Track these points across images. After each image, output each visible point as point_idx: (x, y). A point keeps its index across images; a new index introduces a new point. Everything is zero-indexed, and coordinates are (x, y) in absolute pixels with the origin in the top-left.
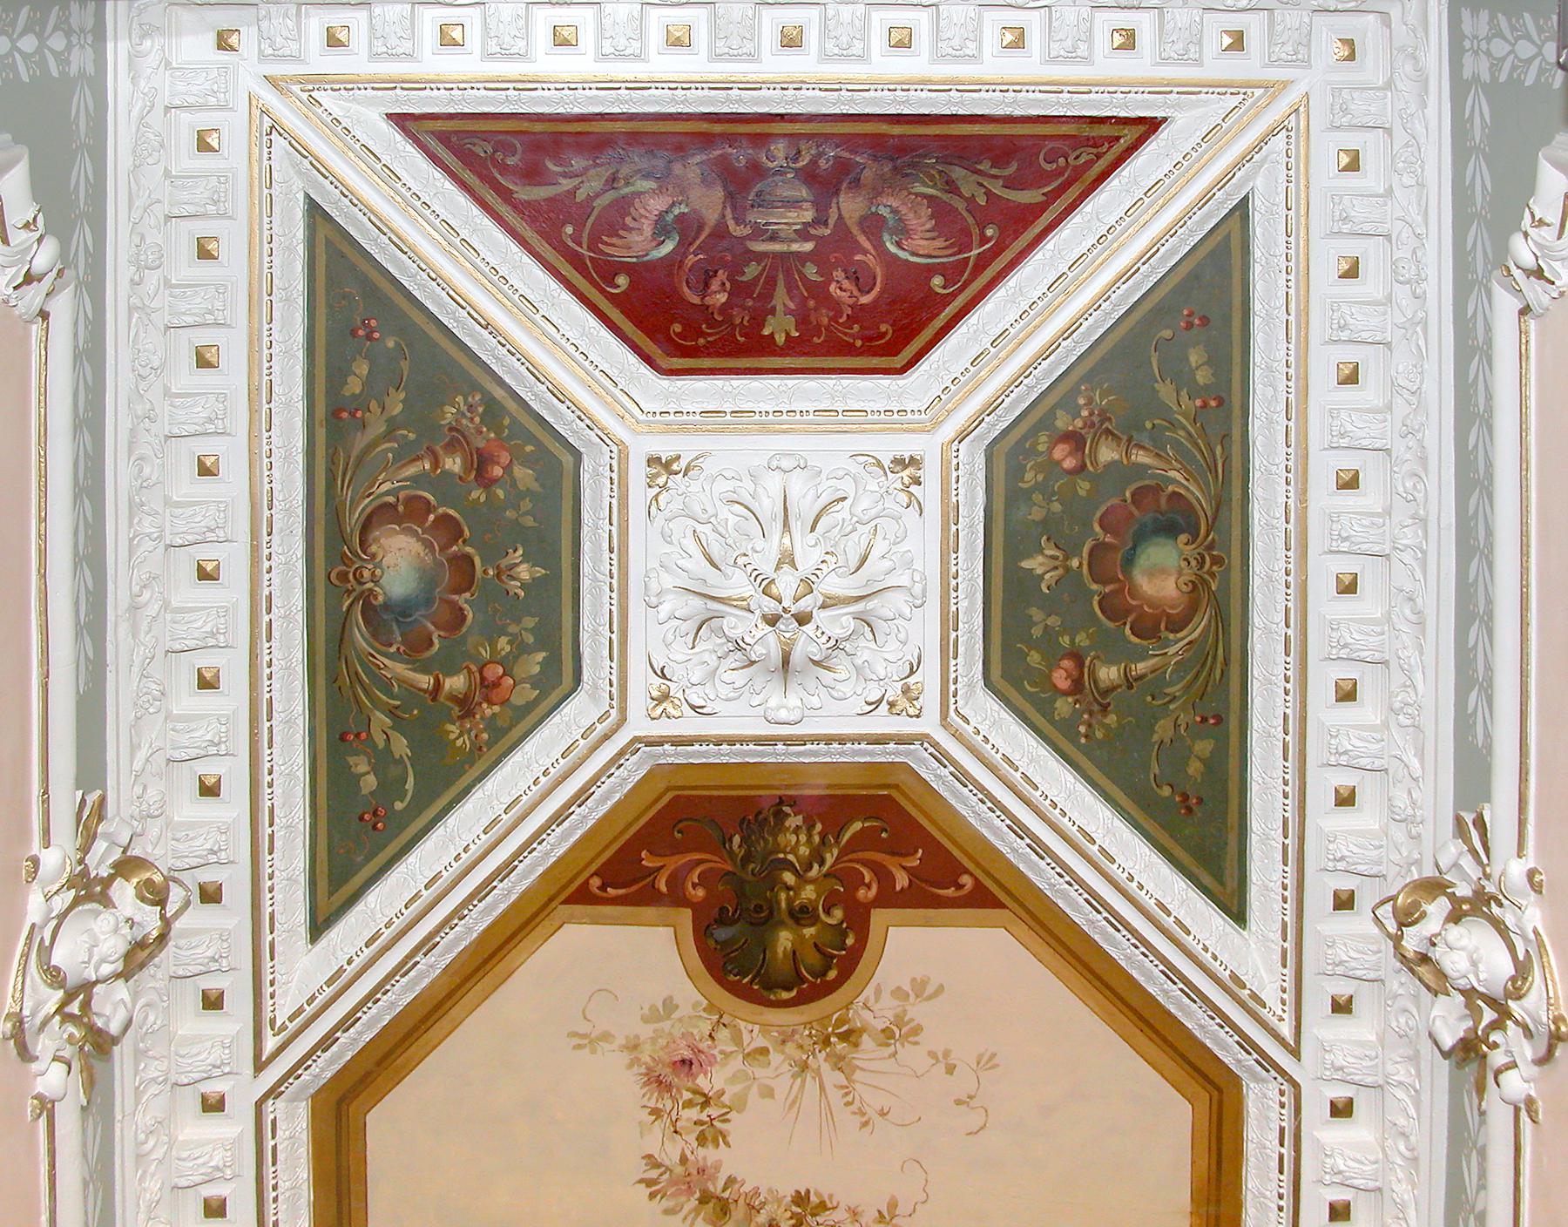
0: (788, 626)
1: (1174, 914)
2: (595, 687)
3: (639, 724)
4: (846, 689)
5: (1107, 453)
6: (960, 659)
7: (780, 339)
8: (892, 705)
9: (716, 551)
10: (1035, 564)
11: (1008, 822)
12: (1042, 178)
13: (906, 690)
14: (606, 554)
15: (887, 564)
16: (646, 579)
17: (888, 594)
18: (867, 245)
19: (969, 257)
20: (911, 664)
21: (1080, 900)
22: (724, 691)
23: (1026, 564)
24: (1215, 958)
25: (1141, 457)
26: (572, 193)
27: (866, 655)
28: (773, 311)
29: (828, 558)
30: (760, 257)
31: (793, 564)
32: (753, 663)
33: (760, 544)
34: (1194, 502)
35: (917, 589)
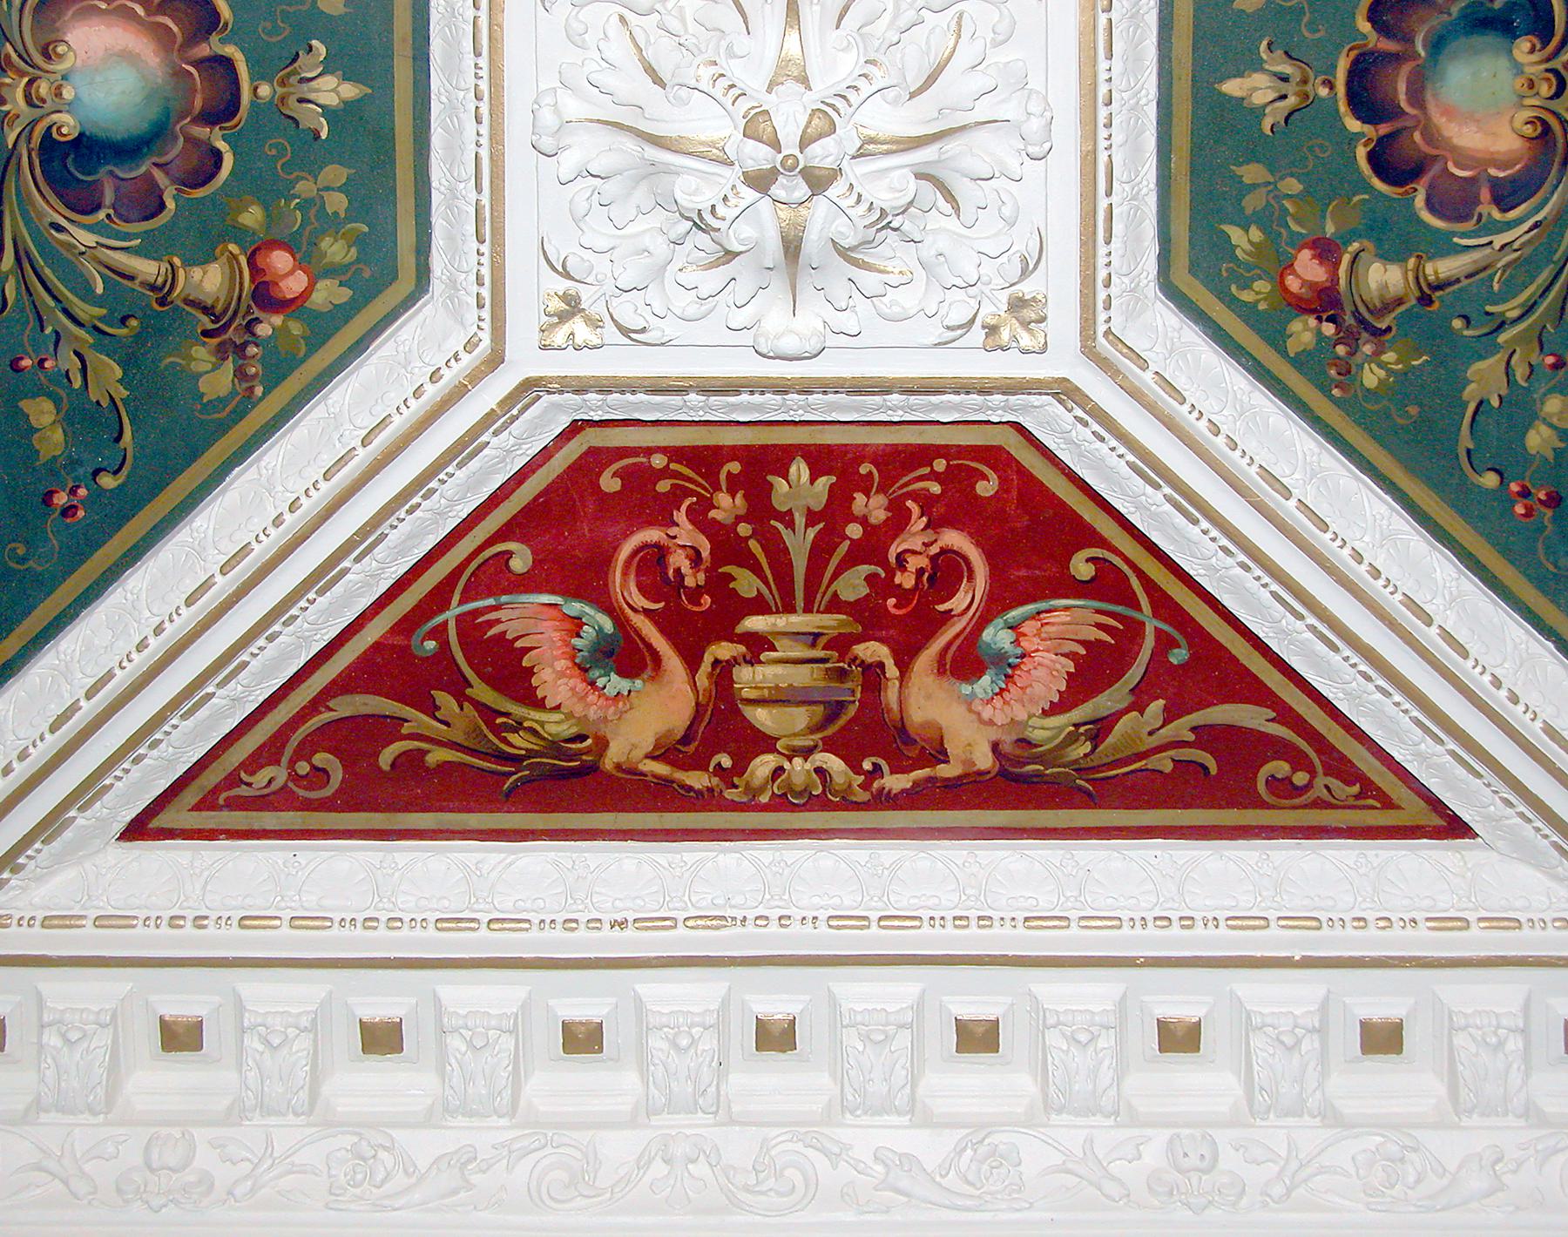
0: (791, 188)
1: (1438, 620)
2: (453, 284)
3: (524, 361)
4: (906, 299)
5: (210, 281)
6: (1116, 243)
7: (800, 469)
8: (992, 330)
9: (665, 57)
10: (331, 91)
11: (1130, 458)
12: (330, 737)
13: (1018, 305)
14: (470, 59)
15: (980, 82)
16: (536, 106)
17: (981, 135)
18: (640, 622)
19: (461, 603)
20: (1024, 260)
21: (1265, 595)
22: (684, 302)
23: (1232, 87)
24: (1514, 699)
25: (148, 269)
26: (1170, 716)
27: (943, 244)
28: (812, 518)
29: (870, 69)
30: (835, 605)
31: (804, 81)
32: (730, 255)
33: (742, 43)
34: (53, 199)
35: (1035, 125)
